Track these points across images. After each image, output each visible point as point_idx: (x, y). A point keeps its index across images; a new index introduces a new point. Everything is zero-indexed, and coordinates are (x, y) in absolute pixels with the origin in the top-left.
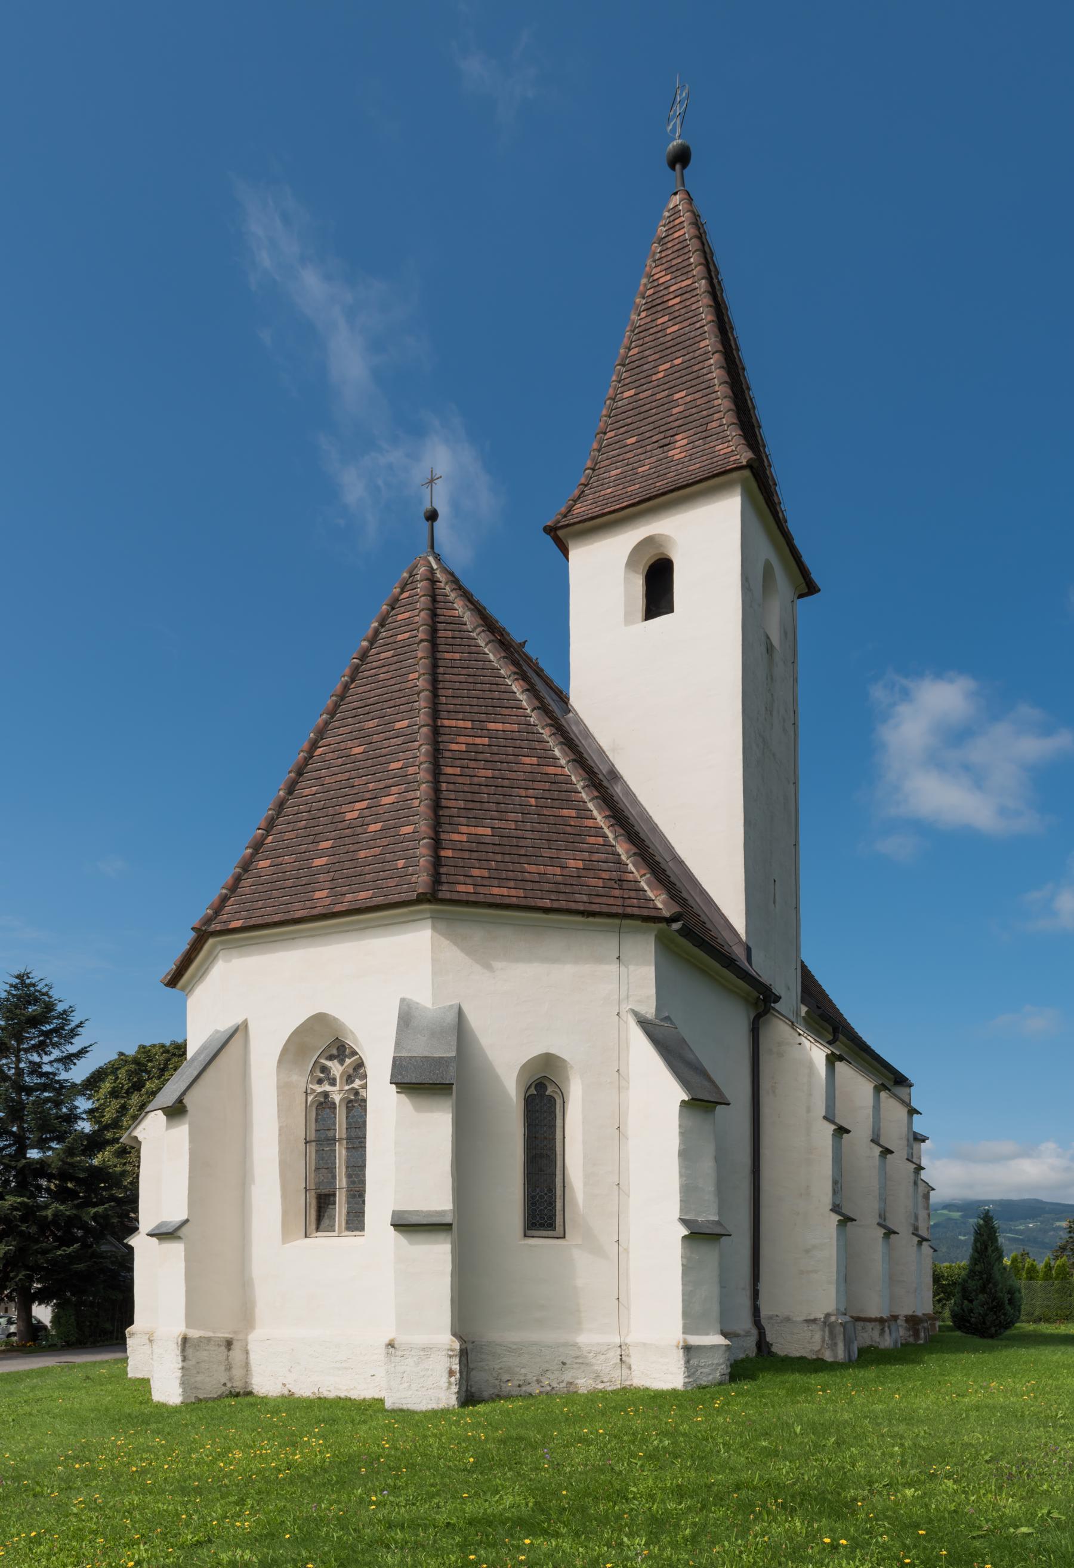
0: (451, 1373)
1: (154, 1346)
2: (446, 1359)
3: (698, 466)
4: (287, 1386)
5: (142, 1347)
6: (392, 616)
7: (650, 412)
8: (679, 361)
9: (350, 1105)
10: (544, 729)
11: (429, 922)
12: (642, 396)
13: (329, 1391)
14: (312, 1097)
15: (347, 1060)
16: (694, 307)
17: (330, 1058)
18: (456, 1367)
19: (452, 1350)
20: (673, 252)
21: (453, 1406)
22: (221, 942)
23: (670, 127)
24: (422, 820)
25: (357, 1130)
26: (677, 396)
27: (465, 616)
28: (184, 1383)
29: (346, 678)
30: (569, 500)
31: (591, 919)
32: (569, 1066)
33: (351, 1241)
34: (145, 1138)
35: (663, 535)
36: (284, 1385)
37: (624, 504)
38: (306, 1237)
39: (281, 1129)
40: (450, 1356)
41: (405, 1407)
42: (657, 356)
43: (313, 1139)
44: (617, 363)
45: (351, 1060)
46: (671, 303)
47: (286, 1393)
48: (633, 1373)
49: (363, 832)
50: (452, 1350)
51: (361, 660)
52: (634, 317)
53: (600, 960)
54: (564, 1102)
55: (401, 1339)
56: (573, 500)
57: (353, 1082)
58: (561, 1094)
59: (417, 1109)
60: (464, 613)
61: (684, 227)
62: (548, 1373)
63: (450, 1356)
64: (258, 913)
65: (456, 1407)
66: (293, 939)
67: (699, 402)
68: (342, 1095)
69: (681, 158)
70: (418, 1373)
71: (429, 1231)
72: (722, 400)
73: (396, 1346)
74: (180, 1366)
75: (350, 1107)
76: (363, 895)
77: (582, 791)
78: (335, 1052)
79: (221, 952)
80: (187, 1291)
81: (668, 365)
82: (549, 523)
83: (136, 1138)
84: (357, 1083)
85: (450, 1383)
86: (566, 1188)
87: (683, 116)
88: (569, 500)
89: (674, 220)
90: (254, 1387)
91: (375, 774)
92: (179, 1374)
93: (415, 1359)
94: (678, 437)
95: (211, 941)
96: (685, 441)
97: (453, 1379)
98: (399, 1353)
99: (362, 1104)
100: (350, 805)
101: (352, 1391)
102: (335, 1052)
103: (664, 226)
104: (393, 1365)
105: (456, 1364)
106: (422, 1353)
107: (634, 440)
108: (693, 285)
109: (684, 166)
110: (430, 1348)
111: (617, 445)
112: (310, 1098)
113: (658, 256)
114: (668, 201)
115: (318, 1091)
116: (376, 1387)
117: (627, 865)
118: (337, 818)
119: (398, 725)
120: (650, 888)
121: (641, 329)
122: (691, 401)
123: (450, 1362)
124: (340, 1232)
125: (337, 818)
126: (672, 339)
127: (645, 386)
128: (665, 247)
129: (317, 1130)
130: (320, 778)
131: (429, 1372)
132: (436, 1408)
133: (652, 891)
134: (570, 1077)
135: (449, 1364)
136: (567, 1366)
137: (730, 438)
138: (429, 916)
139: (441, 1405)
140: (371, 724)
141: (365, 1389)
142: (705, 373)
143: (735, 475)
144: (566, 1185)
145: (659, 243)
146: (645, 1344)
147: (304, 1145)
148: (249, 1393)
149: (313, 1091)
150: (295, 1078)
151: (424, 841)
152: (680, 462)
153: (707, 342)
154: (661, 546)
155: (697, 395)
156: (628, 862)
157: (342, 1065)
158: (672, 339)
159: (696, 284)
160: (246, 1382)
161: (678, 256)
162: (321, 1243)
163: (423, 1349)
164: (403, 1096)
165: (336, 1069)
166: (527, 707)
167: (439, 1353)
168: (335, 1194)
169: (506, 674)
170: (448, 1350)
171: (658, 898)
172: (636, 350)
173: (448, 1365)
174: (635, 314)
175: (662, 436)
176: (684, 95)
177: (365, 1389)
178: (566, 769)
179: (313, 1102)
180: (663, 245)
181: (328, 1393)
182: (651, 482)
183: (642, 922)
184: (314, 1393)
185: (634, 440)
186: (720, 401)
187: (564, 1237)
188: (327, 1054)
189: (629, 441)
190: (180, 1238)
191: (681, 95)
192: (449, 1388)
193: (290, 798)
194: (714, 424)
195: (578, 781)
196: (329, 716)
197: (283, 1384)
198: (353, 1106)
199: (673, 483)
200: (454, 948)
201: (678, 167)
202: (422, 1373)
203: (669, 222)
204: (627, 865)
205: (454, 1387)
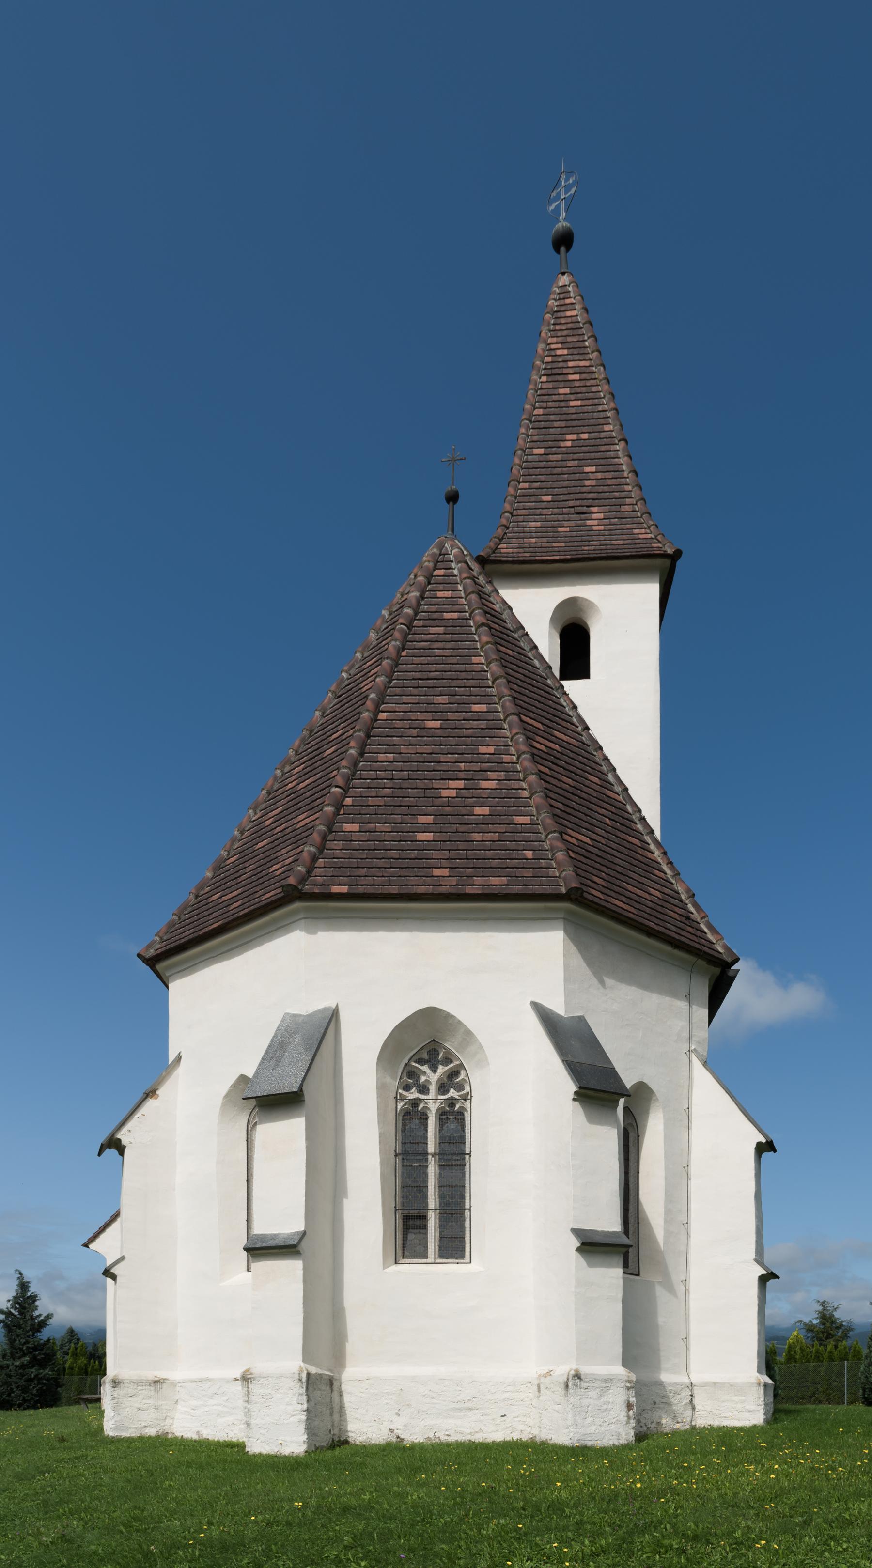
0: (629, 1406)
1: (250, 1386)
2: (623, 1391)
3: (621, 542)
4: (396, 1431)
5: (130, 1399)
6: (430, 591)
7: (562, 476)
8: (585, 436)
9: (444, 1117)
10: (596, 751)
11: (561, 924)
12: (551, 457)
13: (448, 1435)
14: (402, 1104)
15: (440, 1067)
16: (594, 389)
17: (421, 1062)
18: (633, 1400)
19: (629, 1382)
20: (567, 329)
21: (632, 1441)
22: (307, 909)
23: (552, 207)
24: (544, 813)
25: (452, 1145)
26: (587, 469)
27: (505, 613)
28: (311, 1430)
29: (398, 643)
30: (495, 537)
31: (676, 952)
32: (654, 1098)
33: (451, 1268)
34: (131, 1143)
35: (586, 600)
36: (392, 1431)
37: (557, 558)
38: (396, 1263)
39: (380, 1134)
40: (628, 1389)
41: (589, 1444)
42: (563, 424)
43: (400, 1152)
44: (524, 417)
45: (448, 1068)
46: (571, 377)
47: (394, 1439)
48: (697, 1413)
49: (467, 813)
50: (629, 1382)
51: (408, 628)
52: (535, 377)
53: (674, 995)
54: (638, 1136)
55: (584, 1370)
56: (498, 538)
57: (447, 1092)
58: (636, 1128)
59: (590, 1120)
60: (504, 610)
61: (575, 309)
62: (645, 1412)
63: (628, 1389)
64: (363, 880)
65: (634, 1442)
66: (397, 919)
67: (610, 482)
68: (438, 1104)
69: (564, 241)
70: (601, 1406)
71: (606, 1253)
72: (633, 487)
73: (582, 1377)
74: (305, 1407)
75: (443, 1119)
76: (494, 880)
77: (637, 822)
78: (425, 1056)
79: (303, 921)
80: (304, 1318)
81: (575, 437)
82: (482, 554)
83: (120, 1140)
84: (452, 1093)
85: (629, 1417)
86: (640, 1225)
87: (570, 202)
88: (495, 537)
89: (564, 299)
90: (350, 1434)
91: (462, 754)
92: (303, 1417)
93: (598, 1391)
94: (595, 509)
95: (297, 905)
96: (601, 516)
97: (631, 1413)
98: (584, 1385)
99: (458, 1117)
100: (442, 781)
101: (476, 1434)
102: (425, 1056)
103: (555, 300)
104: (579, 1398)
105: (633, 1397)
106: (604, 1385)
107: (549, 498)
108: (591, 368)
109: (568, 248)
110: (612, 1380)
111: (533, 498)
112: (400, 1105)
113: (552, 327)
114: (555, 279)
115: (409, 1098)
116: (507, 1428)
117: (687, 905)
118: (429, 793)
119: (475, 708)
120: (710, 931)
121: (543, 392)
122: (601, 479)
123: (628, 1395)
124: (435, 1259)
125: (429, 793)
126: (576, 413)
127: (554, 449)
128: (558, 321)
129: (403, 1143)
130: (394, 745)
131: (610, 1406)
132: (616, 1443)
133: (712, 935)
134: (651, 1111)
135: (627, 1396)
136: (657, 1406)
137: (645, 525)
138: (562, 916)
139: (623, 1441)
140: (440, 699)
141: (493, 1432)
142: (612, 456)
143: (658, 562)
144: (640, 1221)
145: (552, 315)
146: (715, 1384)
147: (394, 1157)
148: (346, 1442)
149: (403, 1098)
150: (388, 1080)
151: (555, 834)
152: (599, 534)
153: (611, 427)
154: (581, 610)
155: (607, 475)
156: (687, 902)
157: (435, 1072)
158: (576, 413)
159: (594, 368)
160: (340, 1430)
161: (573, 335)
162: (411, 1269)
163: (605, 1381)
164: (577, 1104)
165: (432, 1077)
166: (578, 725)
167: (618, 1385)
168: (424, 1218)
169: (554, 685)
170: (626, 1381)
171: (719, 942)
172: (541, 411)
173: (625, 1398)
174: (537, 375)
175: (578, 503)
176: (571, 181)
177: (493, 1432)
178: (621, 797)
179: (401, 1110)
180: (556, 318)
181: (446, 1438)
182: (576, 544)
183: (707, 963)
184: (429, 1438)
185: (549, 498)
186: (630, 488)
187: (638, 1275)
188: (416, 1058)
189: (545, 498)
190: (298, 1253)
191: (566, 180)
192: (628, 1423)
193: (361, 760)
194: (627, 508)
195: (635, 812)
196: (387, 680)
197: (390, 1430)
198: (448, 1119)
199: (599, 552)
200: (579, 956)
201: (563, 249)
202: (605, 1407)
203: (560, 299)
204: (687, 905)
205: (632, 1421)
